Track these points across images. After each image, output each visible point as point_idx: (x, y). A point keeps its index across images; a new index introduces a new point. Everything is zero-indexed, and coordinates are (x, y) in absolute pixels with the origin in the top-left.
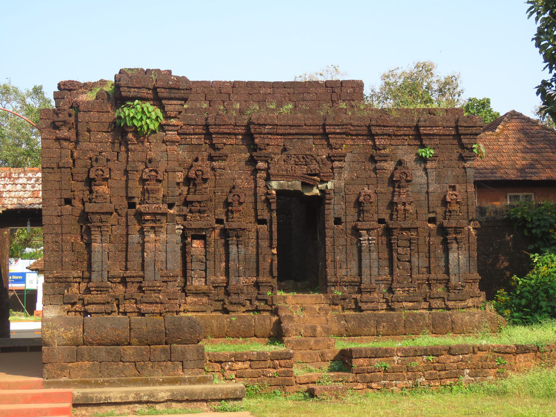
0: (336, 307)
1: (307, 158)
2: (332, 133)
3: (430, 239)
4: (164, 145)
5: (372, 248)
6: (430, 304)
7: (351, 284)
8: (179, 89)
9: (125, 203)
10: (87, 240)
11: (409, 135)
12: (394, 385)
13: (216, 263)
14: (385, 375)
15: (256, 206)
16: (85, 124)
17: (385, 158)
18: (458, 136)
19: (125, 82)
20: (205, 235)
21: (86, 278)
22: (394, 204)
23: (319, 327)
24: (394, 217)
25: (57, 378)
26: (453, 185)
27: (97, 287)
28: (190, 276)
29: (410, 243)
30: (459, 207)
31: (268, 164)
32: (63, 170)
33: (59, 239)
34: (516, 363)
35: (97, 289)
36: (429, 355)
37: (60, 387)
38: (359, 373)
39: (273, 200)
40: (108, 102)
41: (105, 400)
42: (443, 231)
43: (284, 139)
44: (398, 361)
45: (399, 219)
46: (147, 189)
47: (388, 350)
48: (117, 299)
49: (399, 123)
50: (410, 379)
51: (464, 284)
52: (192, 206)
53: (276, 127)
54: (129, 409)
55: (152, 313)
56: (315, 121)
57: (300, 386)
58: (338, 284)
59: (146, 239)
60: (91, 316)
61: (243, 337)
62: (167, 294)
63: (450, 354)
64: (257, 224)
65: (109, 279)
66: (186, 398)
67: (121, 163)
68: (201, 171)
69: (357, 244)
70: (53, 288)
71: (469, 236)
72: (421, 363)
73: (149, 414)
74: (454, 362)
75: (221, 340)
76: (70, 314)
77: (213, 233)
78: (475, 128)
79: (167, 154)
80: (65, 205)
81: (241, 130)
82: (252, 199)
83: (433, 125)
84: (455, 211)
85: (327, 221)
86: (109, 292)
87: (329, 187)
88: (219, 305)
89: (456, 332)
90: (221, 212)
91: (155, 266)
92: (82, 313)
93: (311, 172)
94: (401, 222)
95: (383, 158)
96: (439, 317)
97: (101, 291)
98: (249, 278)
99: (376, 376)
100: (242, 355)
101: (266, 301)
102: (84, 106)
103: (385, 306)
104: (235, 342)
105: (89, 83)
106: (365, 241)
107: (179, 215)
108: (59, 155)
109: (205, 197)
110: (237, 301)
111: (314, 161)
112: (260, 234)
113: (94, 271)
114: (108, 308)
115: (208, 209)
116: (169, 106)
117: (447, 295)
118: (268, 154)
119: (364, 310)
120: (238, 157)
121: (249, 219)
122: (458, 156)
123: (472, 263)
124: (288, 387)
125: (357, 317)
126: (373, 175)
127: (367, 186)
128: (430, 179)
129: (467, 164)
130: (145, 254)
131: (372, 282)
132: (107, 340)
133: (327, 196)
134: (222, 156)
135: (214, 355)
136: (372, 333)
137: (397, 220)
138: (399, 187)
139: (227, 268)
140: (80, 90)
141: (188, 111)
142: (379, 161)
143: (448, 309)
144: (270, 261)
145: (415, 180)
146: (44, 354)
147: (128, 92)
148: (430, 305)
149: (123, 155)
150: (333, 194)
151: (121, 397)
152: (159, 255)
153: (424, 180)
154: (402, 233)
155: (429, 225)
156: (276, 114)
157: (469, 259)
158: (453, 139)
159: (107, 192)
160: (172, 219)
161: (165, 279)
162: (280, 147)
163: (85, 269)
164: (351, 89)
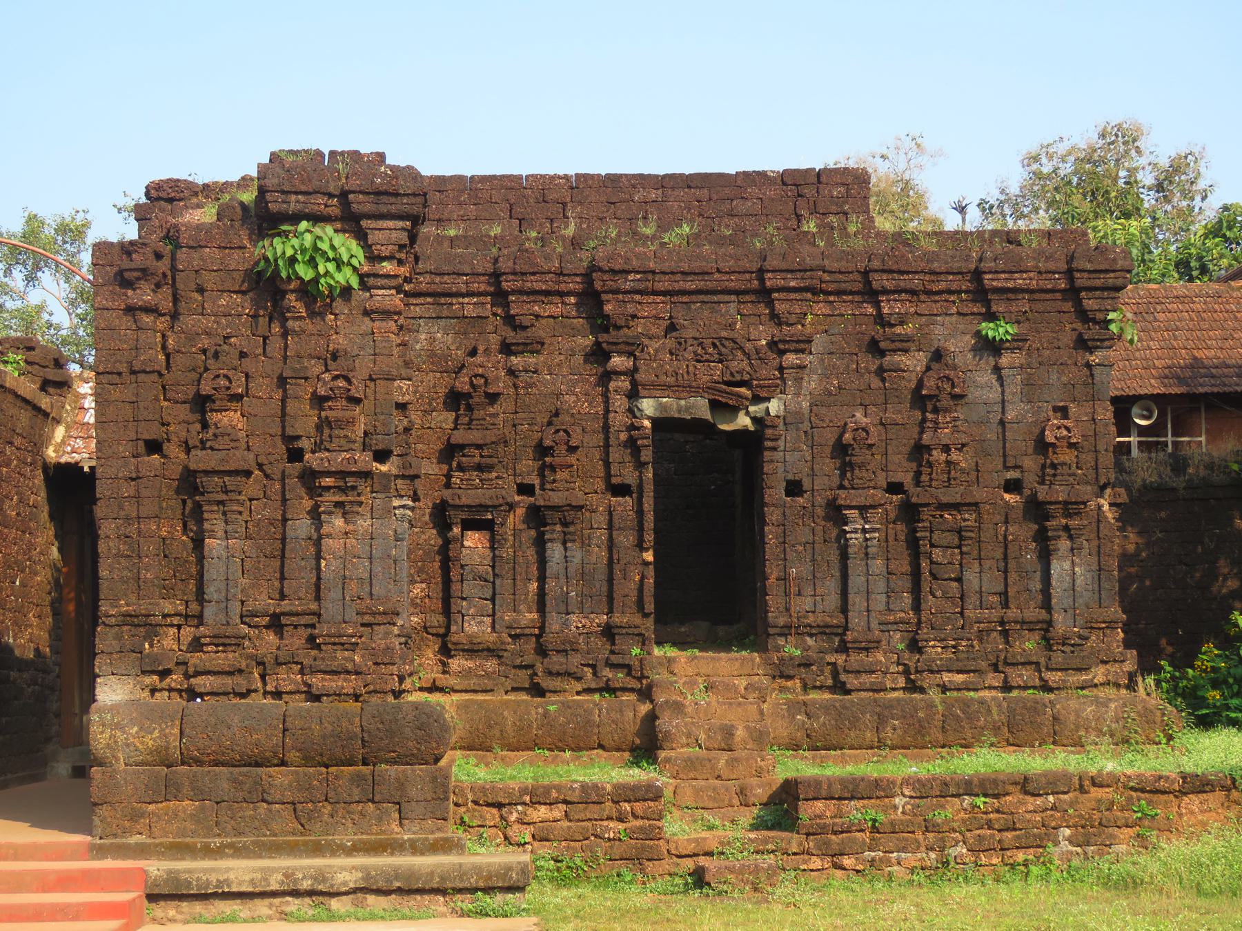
0: (789, 684)
1: (724, 346)
2: (780, 290)
3: (1007, 528)
4: (367, 320)
5: (871, 550)
6: (1006, 677)
7: (823, 631)
8: (397, 195)
9: (281, 448)
10: (195, 533)
11: (959, 292)
12: (893, 861)
13: (518, 583)
14: (873, 839)
15: (607, 454)
16: (193, 275)
17: (904, 345)
18: (1073, 293)
19: (275, 181)
20: (493, 520)
21: (194, 616)
22: (924, 450)
23: (740, 728)
24: (925, 478)
25: (123, 837)
26: (1062, 404)
27: (215, 637)
28: (459, 612)
29: (961, 538)
30: (1077, 456)
31: (635, 359)
32: (142, 377)
33: (132, 530)
34: (1180, 815)
35: (216, 641)
36: (977, 795)
37: (125, 857)
38: (814, 834)
39: (646, 442)
40: (242, 225)
41: (217, 887)
42: (1037, 510)
43: (671, 302)
44: (903, 807)
45: (933, 484)
46: (327, 417)
47: (882, 781)
48: (261, 663)
49: (936, 265)
50: (932, 849)
51: (1084, 632)
52: (464, 456)
53: (650, 277)
54: (270, 908)
55: (335, 694)
56: (740, 263)
57: (679, 861)
58: (793, 631)
59: (325, 529)
60: (203, 700)
61: (573, 750)
62: (372, 652)
63: (1026, 793)
64: (609, 496)
65: (244, 619)
66: (398, 884)
67: (271, 361)
68: (482, 376)
69: (838, 540)
70: (119, 637)
71: (1099, 521)
72: (958, 812)
73: (314, 919)
74: (1035, 812)
75: (523, 756)
76: (157, 695)
77: (512, 516)
78: (1112, 275)
79: (374, 341)
80: (149, 455)
81: (574, 285)
82: (598, 439)
83: (1014, 269)
84: (1065, 464)
85: (769, 488)
86: (244, 648)
87: (773, 412)
88: (523, 677)
89: (1065, 743)
90: (528, 469)
91: (343, 589)
92: (183, 694)
93: (731, 379)
94: (939, 491)
95: (899, 345)
96: (1025, 707)
97: (224, 645)
98: (592, 616)
99: (854, 841)
100: (547, 789)
101: (628, 668)
102: (190, 236)
103: (901, 682)
104: (554, 760)
105: (213, 183)
106: (856, 532)
107: (403, 477)
108: (132, 343)
109: (490, 436)
110: (562, 669)
111: (739, 353)
112: (615, 518)
113: (210, 602)
114: (241, 683)
115: (500, 462)
116: (377, 232)
117: (1045, 656)
118: (634, 337)
119: (853, 691)
120: (567, 346)
121: (593, 484)
122: (1074, 337)
123: (1105, 585)
124: (650, 864)
125: (834, 707)
126: (876, 383)
127: (861, 409)
128: (1007, 391)
129: (1095, 358)
130: (323, 563)
131: (872, 626)
132: (232, 754)
133: (769, 432)
134: (532, 344)
135: (483, 789)
136: (867, 743)
137: (930, 486)
138: (936, 410)
139: (541, 594)
140: (194, 200)
141: (458, 242)
142: (889, 351)
143: (1047, 688)
144: (638, 578)
145: (974, 394)
146: (94, 783)
147: (283, 202)
148: (1005, 681)
149: (275, 344)
150: (781, 427)
151: (252, 881)
152: (353, 564)
153: (994, 395)
154: (942, 516)
155: (1007, 496)
156: (652, 248)
157: (1099, 575)
158: (1063, 300)
159: (240, 426)
160: (384, 485)
161: (367, 619)
162: (661, 322)
163: (192, 597)
164: (842, 189)
